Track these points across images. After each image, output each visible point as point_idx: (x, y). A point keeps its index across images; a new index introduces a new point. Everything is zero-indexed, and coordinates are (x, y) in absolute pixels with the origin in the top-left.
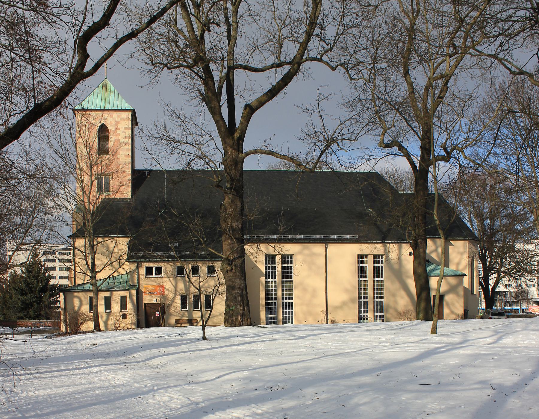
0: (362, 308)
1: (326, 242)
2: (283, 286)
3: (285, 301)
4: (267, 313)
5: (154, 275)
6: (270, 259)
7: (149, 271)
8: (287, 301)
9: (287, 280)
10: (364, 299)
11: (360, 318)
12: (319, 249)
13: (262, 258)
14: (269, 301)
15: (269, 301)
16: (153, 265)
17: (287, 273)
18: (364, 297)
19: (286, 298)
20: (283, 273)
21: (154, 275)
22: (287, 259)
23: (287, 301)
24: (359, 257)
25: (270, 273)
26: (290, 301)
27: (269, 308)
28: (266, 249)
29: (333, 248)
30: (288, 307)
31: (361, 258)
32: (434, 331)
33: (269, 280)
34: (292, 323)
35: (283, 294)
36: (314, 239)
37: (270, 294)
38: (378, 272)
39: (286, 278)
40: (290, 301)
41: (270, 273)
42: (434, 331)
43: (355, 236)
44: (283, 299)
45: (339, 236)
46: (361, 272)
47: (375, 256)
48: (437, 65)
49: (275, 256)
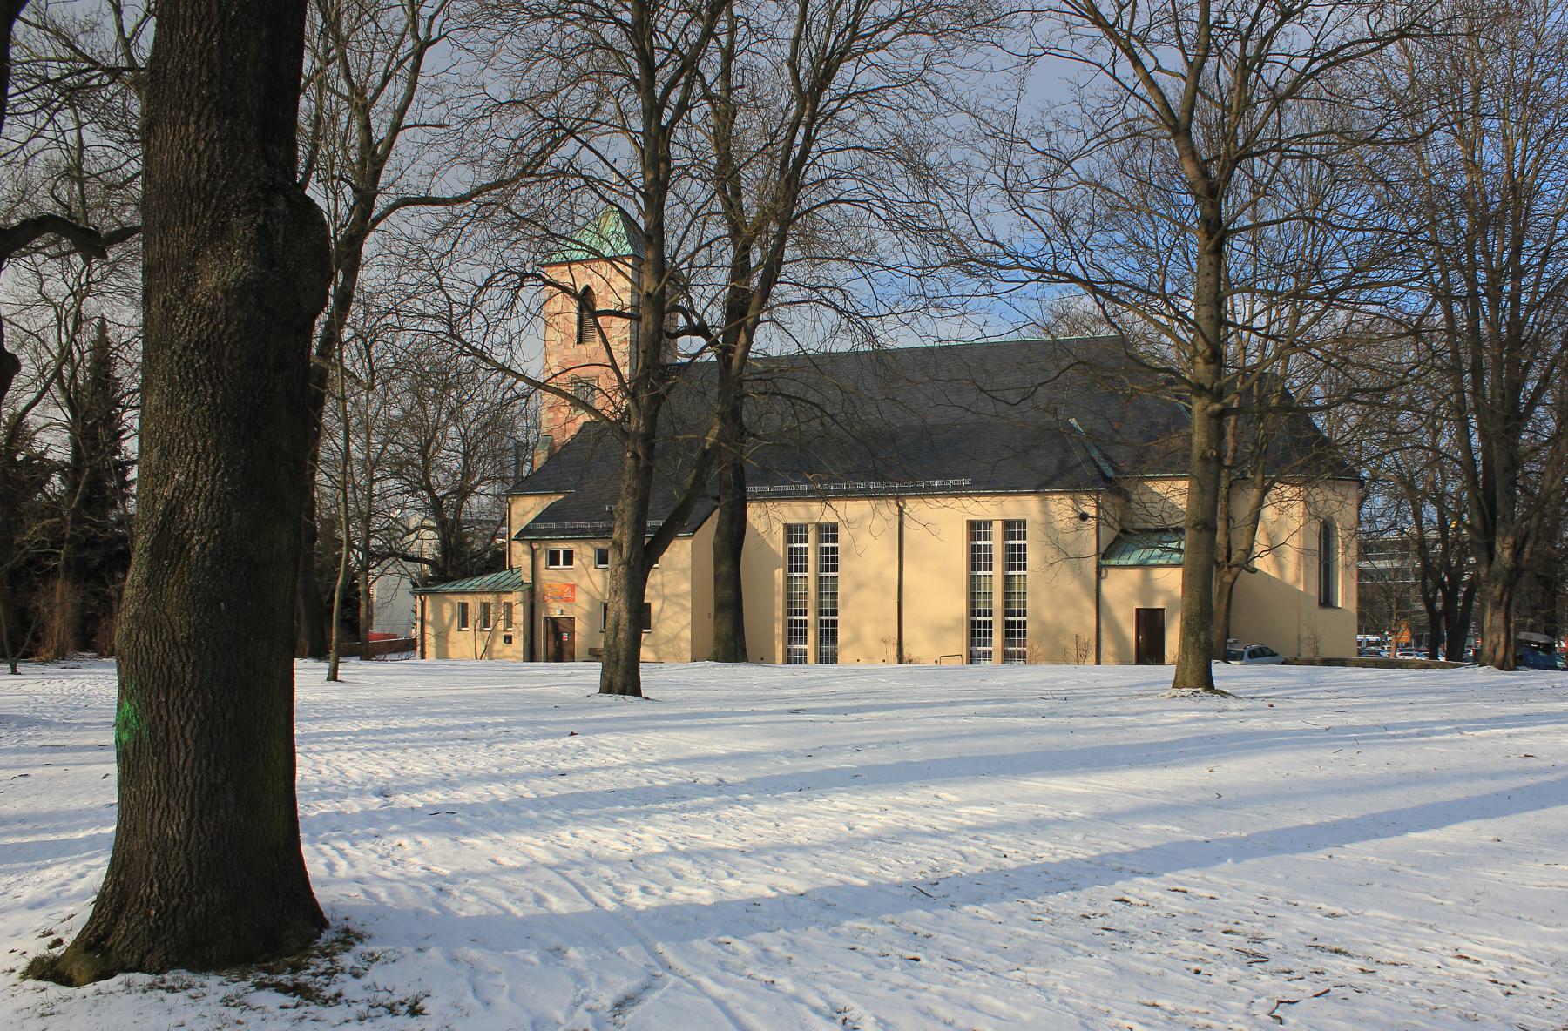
0: (978, 632)
1: (899, 496)
2: (1006, 587)
3: (1010, 618)
4: (1006, 643)
5: (561, 566)
6: (794, 532)
7: (553, 558)
8: (1016, 618)
9: (1016, 573)
10: (985, 615)
11: (972, 659)
12: (889, 509)
13: (779, 533)
14: (979, 618)
15: (979, 618)
16: (561, 547)
17: (829, 560)
18: (1019, 611)
19: (1013, 611)
20: (790, 561)
21: (561, 566)
22: (828, 532)
23: (1016, 618)
24: (973, 525)
25: (795, 562)
26: (988, 618)
27: (796, 631)
28: (795, 512)
29: (913, 506)
30: (828, 631)
31: (977, 529)
32: (333, 676)
33: (979, 573)
34: (423, 657)
35: (1006, 604)
36: (778, 493)
37: (794, 605)
38: (1016, 558)
39: (1013, 569)
40: (988, 618)
41: (795, 562)
42: (333, 676)
43: (968, 482)
44: (1006, 613)
45: (788, 488)
46: (978, 559)
47: (1006, 523)
48: (1160, 84)
49: (991, 523)
